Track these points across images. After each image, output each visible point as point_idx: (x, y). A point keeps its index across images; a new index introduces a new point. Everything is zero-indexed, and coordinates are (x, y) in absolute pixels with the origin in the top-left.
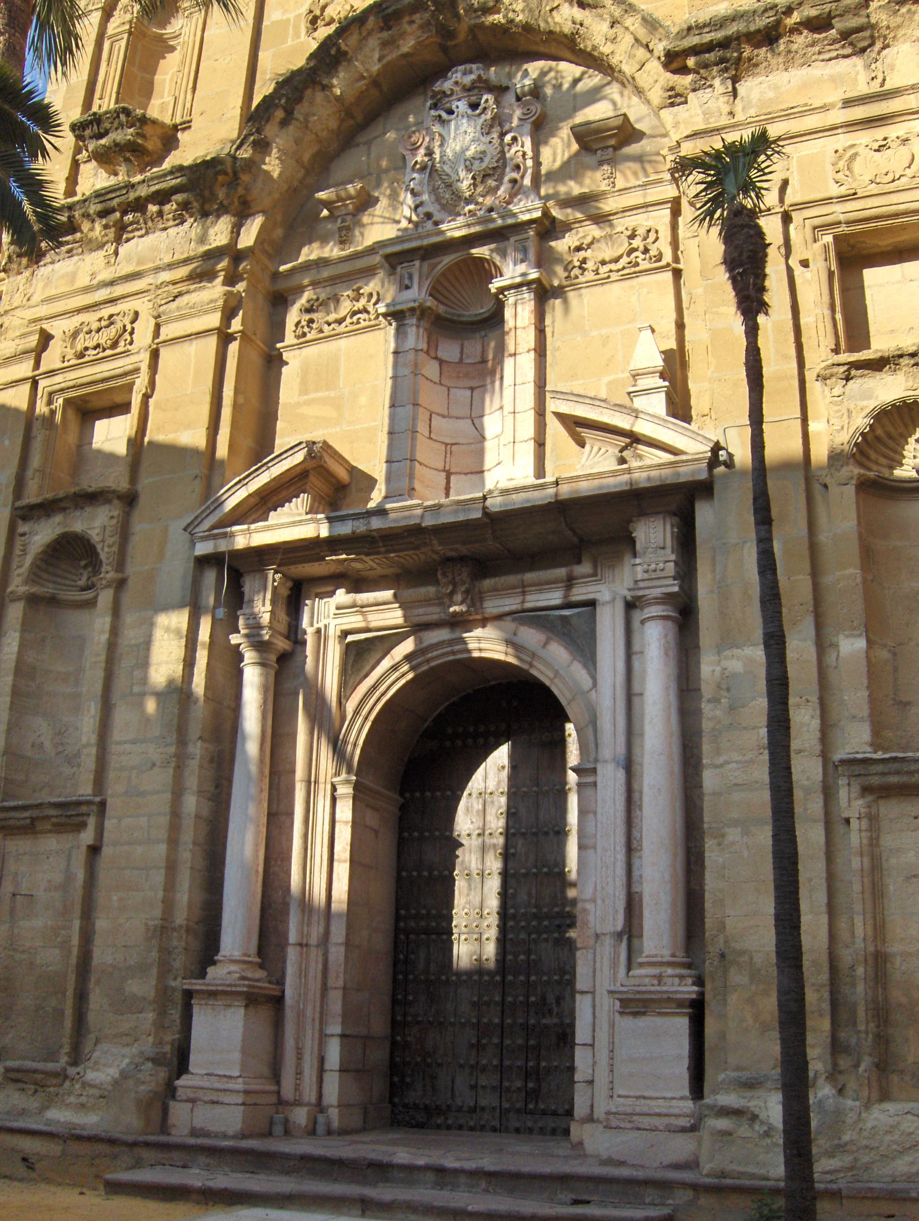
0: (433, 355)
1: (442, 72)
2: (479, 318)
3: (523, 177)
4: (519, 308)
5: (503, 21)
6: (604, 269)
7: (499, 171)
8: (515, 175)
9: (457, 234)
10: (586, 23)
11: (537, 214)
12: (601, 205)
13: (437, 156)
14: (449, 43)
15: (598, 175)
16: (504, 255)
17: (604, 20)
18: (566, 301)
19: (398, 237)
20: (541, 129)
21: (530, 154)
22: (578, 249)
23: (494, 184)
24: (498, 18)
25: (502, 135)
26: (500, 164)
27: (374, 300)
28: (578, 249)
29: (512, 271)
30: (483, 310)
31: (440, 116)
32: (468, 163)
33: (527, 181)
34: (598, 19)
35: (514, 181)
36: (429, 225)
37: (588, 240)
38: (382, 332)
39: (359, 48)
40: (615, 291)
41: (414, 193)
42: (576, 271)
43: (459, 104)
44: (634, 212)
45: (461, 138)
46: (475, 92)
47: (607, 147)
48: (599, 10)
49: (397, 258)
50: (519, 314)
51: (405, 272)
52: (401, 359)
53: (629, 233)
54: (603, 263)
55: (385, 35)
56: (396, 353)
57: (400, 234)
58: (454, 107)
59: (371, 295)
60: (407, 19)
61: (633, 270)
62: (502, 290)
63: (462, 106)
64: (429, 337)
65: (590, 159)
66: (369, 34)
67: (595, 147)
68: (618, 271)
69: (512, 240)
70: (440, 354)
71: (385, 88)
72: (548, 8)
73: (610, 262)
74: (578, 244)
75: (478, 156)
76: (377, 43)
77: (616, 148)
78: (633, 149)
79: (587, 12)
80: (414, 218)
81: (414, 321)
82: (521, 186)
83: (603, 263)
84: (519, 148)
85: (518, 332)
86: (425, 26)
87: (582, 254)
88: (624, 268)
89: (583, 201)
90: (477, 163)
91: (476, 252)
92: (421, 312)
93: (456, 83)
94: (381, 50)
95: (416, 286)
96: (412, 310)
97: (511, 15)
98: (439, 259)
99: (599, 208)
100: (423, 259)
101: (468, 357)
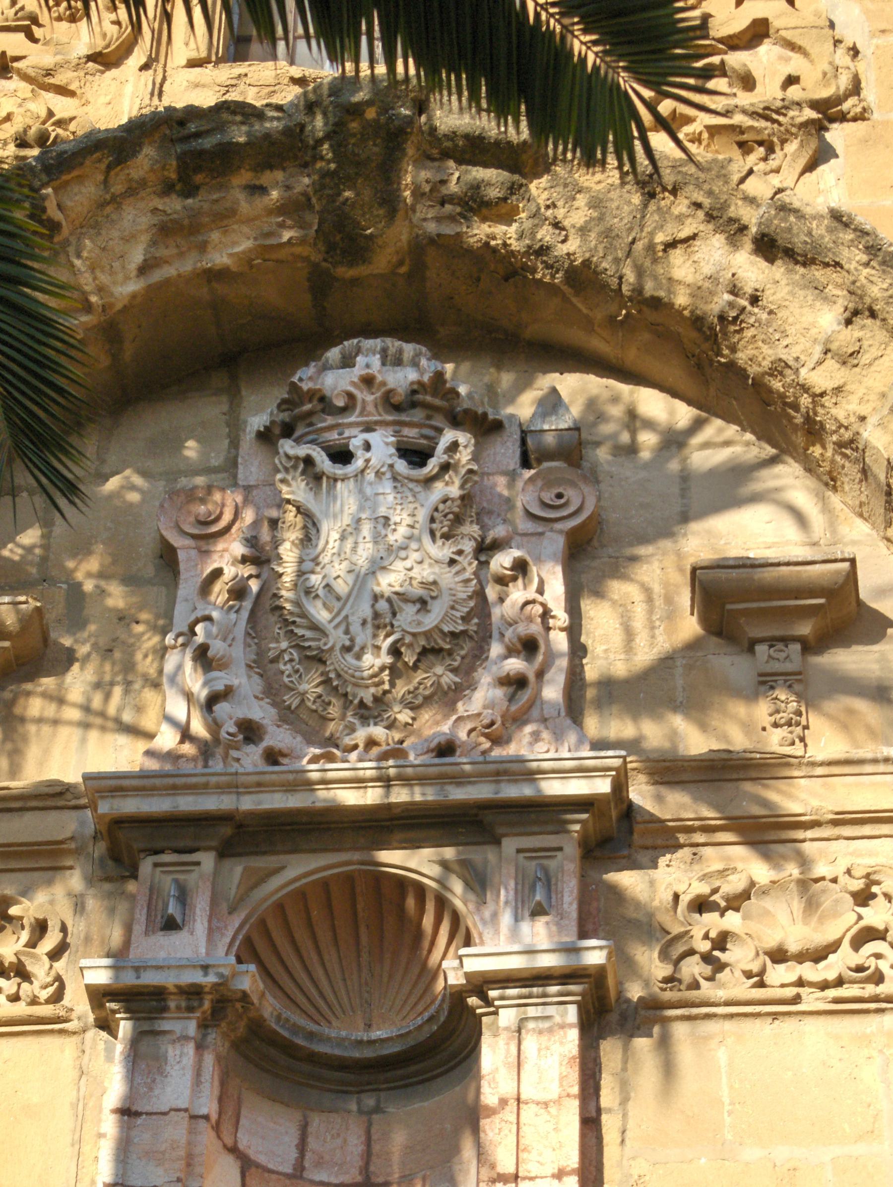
0: (229, 1142)
1: (310, 339)
2: (368, 1053)
3: (540, 674)
4: (530, 1042)
5: (515, 245)
6: (779, 974)
7: (467, 647)
8: (515, 665)
9: (350, 797)
10: (770, 297)
11: (603, 786)
12: (773, 796)
13: (288, 568)
14: (345, 272)
15: (762, 711)
16: (479, 883)
17: (829, 300)
18: (665, 1044)
19: (143, 775)
20: (591, 556)
21: (561, 617)
22: (701, 905)
23: (448, 679)
24: (507, 234)
25: (486, 549)
26: (472, 626)
27: (49, 943)
28: (701, 905)
29: (504, 939)
30: (386, 1029)
31: (308, 461)
32: (382, 605)
33: (552, 692)
34: (810, 295)
35: (517, 683)
36: (251, 758)
37: (734, 884)
38: (69, 1045)
39: (92, 223)
40: (813, 1042)
41: (203, 657)
42: (693, 968)
43: (375, 438)
44: (867, 830)
45: (369, 537)
46: (418, 415)
47: (785, 640)
48: (818, 274)
49: (131, 839)
50: (527, 1064)
51: (167, 883)
52: (143, 1137)
53: (857, 885)
54: (779, 956)
55: (174, 205)
56: (127, 1112)
57: (153, 765)
58: (355, 444)
59: (41, 928)
60: (244, 177)
61: (870, 989)
62: (481, 984)
63: (378, 448)
64: (223, 1084)
65: (732, 665)
66: (133, 190)
67: (755, 632)
68: (824, 986)
69: (510, 845)
70: (244, 1142)
71: (128, 352)
72: (660, 238)
73: (801, 957)
74: (703, 889)
75: (419, 592)
76: (145, 221)
77: (809, 647)
78: (854, 660)
79: (778, 270)
80: (198, 728)
81: (191, 1027)
82: (537, 697)
83: (779, 956)
84: (531, 594)
85: (527, 1113)
86: (293, 209)
87: (712, 922)
88: (840, 982)
89: (721, 773)
90: (408, 612)
91: (393, 858)
92: (216, 1007)
93: (368, 381)
94: (154, 243)
95: (200, 926)
96: (193, 993)
97: (545, 234)
98: (271, 861)
99: (765, 803)
100: (226, 851)
101: (319, 1164)
